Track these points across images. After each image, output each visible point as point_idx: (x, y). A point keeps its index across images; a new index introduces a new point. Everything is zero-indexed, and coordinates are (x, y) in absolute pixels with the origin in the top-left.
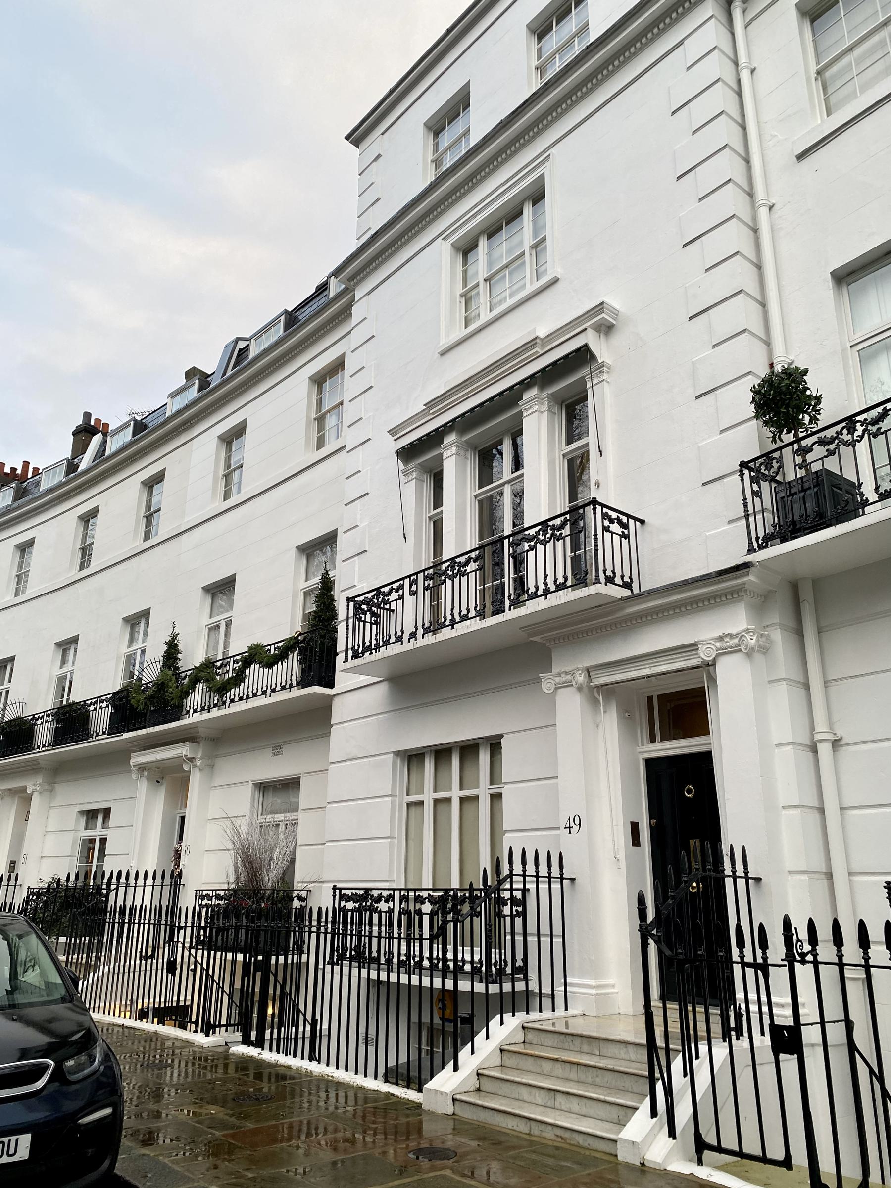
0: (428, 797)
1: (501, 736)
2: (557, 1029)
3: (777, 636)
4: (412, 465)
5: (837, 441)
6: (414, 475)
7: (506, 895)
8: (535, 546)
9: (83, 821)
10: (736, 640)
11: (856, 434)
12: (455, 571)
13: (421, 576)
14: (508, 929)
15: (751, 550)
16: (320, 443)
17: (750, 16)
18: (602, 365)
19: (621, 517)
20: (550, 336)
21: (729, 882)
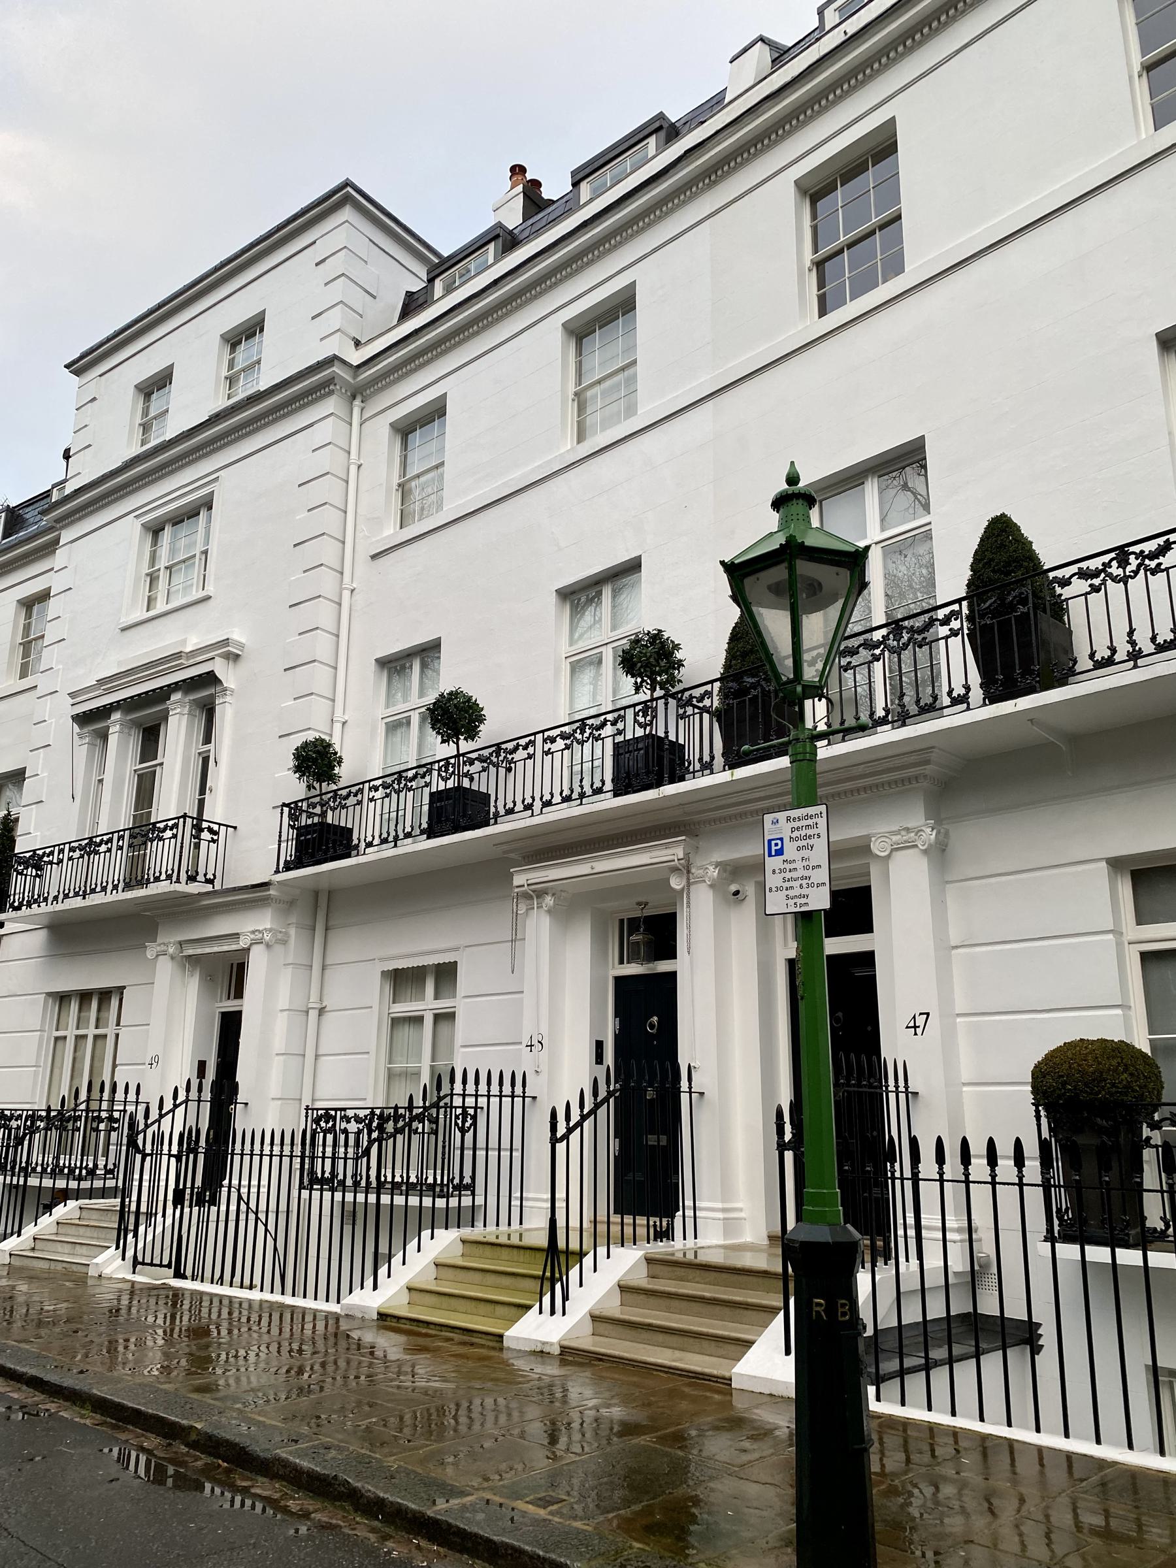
0: (71, 1032)
1: (124, 987)
2: (499, 1241)
3: (292, 931)
4: (86, 730)
5: (1103, 575)
6: (87, 740)
7: (104, 1115)
8: (1104, 582)
9: (388, 989)
10: (912, 834)
11: (1129, 568)
12: (586, 735)
13: (539, 737)
14: (458, 1144)
15: (277, 872)
16: (150, 602)
17: (366, 416)
18: (225, 690)
19: (212, 825)
20: (193, 653)
21: (892, 1096)
